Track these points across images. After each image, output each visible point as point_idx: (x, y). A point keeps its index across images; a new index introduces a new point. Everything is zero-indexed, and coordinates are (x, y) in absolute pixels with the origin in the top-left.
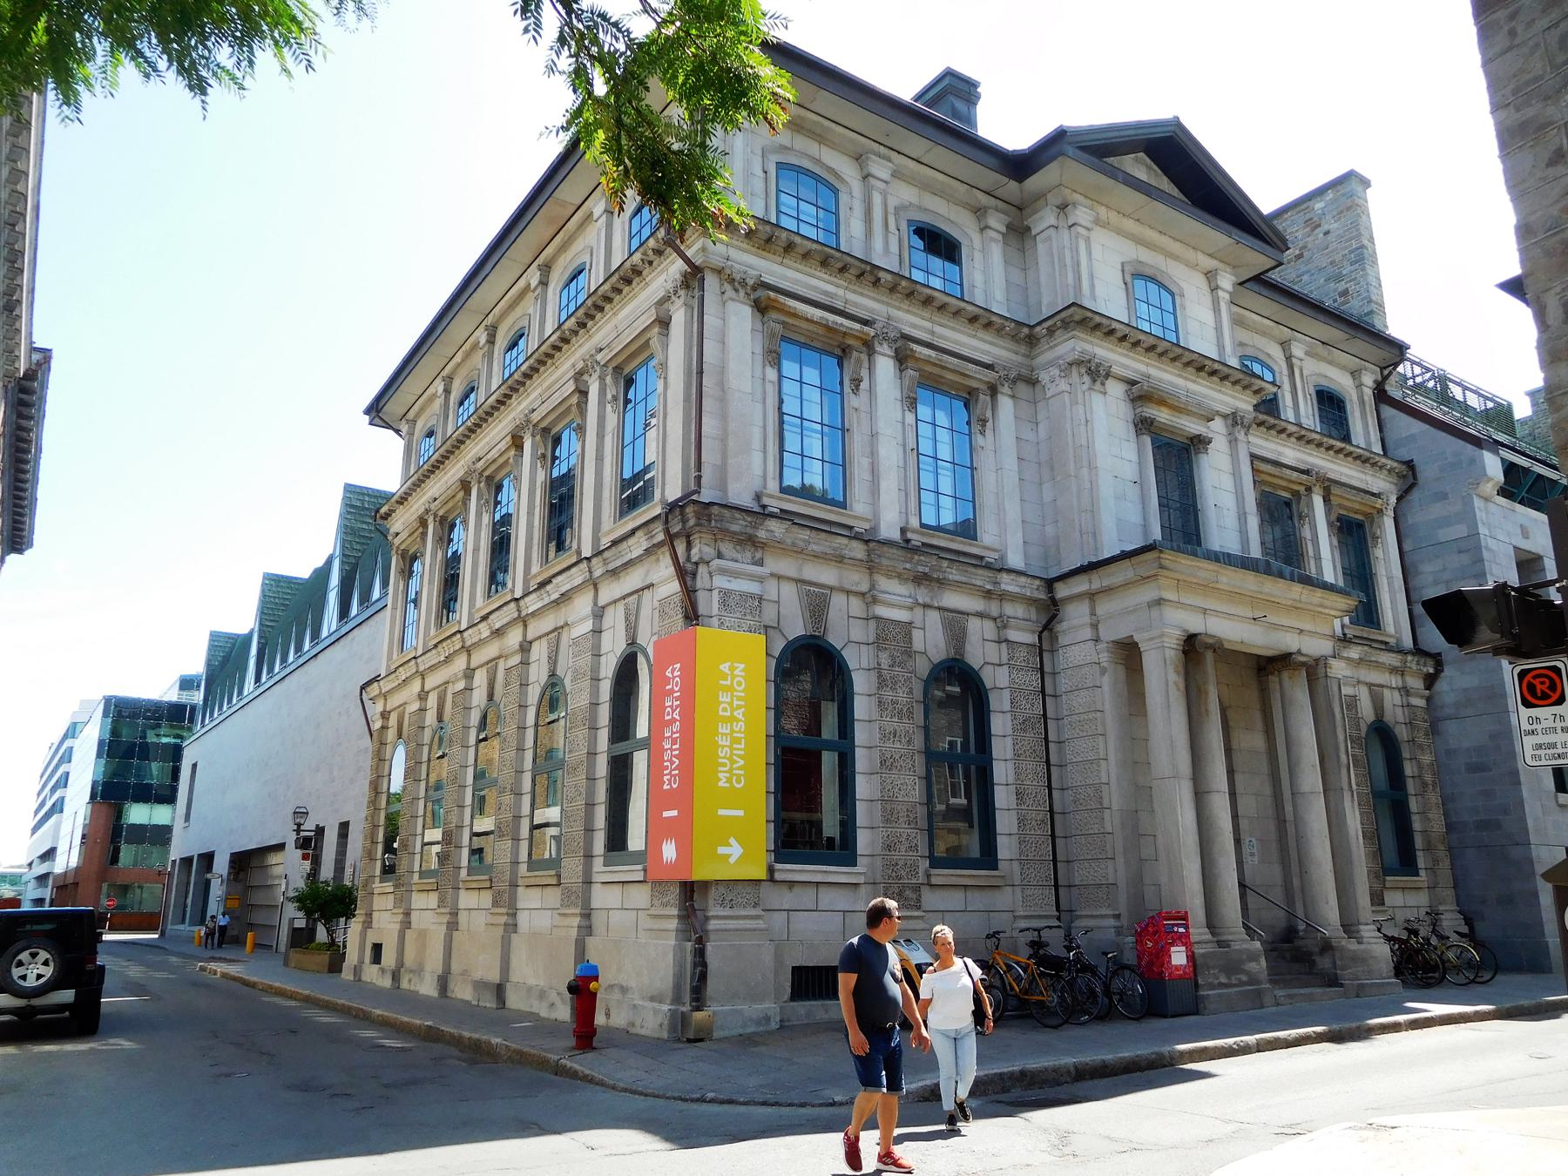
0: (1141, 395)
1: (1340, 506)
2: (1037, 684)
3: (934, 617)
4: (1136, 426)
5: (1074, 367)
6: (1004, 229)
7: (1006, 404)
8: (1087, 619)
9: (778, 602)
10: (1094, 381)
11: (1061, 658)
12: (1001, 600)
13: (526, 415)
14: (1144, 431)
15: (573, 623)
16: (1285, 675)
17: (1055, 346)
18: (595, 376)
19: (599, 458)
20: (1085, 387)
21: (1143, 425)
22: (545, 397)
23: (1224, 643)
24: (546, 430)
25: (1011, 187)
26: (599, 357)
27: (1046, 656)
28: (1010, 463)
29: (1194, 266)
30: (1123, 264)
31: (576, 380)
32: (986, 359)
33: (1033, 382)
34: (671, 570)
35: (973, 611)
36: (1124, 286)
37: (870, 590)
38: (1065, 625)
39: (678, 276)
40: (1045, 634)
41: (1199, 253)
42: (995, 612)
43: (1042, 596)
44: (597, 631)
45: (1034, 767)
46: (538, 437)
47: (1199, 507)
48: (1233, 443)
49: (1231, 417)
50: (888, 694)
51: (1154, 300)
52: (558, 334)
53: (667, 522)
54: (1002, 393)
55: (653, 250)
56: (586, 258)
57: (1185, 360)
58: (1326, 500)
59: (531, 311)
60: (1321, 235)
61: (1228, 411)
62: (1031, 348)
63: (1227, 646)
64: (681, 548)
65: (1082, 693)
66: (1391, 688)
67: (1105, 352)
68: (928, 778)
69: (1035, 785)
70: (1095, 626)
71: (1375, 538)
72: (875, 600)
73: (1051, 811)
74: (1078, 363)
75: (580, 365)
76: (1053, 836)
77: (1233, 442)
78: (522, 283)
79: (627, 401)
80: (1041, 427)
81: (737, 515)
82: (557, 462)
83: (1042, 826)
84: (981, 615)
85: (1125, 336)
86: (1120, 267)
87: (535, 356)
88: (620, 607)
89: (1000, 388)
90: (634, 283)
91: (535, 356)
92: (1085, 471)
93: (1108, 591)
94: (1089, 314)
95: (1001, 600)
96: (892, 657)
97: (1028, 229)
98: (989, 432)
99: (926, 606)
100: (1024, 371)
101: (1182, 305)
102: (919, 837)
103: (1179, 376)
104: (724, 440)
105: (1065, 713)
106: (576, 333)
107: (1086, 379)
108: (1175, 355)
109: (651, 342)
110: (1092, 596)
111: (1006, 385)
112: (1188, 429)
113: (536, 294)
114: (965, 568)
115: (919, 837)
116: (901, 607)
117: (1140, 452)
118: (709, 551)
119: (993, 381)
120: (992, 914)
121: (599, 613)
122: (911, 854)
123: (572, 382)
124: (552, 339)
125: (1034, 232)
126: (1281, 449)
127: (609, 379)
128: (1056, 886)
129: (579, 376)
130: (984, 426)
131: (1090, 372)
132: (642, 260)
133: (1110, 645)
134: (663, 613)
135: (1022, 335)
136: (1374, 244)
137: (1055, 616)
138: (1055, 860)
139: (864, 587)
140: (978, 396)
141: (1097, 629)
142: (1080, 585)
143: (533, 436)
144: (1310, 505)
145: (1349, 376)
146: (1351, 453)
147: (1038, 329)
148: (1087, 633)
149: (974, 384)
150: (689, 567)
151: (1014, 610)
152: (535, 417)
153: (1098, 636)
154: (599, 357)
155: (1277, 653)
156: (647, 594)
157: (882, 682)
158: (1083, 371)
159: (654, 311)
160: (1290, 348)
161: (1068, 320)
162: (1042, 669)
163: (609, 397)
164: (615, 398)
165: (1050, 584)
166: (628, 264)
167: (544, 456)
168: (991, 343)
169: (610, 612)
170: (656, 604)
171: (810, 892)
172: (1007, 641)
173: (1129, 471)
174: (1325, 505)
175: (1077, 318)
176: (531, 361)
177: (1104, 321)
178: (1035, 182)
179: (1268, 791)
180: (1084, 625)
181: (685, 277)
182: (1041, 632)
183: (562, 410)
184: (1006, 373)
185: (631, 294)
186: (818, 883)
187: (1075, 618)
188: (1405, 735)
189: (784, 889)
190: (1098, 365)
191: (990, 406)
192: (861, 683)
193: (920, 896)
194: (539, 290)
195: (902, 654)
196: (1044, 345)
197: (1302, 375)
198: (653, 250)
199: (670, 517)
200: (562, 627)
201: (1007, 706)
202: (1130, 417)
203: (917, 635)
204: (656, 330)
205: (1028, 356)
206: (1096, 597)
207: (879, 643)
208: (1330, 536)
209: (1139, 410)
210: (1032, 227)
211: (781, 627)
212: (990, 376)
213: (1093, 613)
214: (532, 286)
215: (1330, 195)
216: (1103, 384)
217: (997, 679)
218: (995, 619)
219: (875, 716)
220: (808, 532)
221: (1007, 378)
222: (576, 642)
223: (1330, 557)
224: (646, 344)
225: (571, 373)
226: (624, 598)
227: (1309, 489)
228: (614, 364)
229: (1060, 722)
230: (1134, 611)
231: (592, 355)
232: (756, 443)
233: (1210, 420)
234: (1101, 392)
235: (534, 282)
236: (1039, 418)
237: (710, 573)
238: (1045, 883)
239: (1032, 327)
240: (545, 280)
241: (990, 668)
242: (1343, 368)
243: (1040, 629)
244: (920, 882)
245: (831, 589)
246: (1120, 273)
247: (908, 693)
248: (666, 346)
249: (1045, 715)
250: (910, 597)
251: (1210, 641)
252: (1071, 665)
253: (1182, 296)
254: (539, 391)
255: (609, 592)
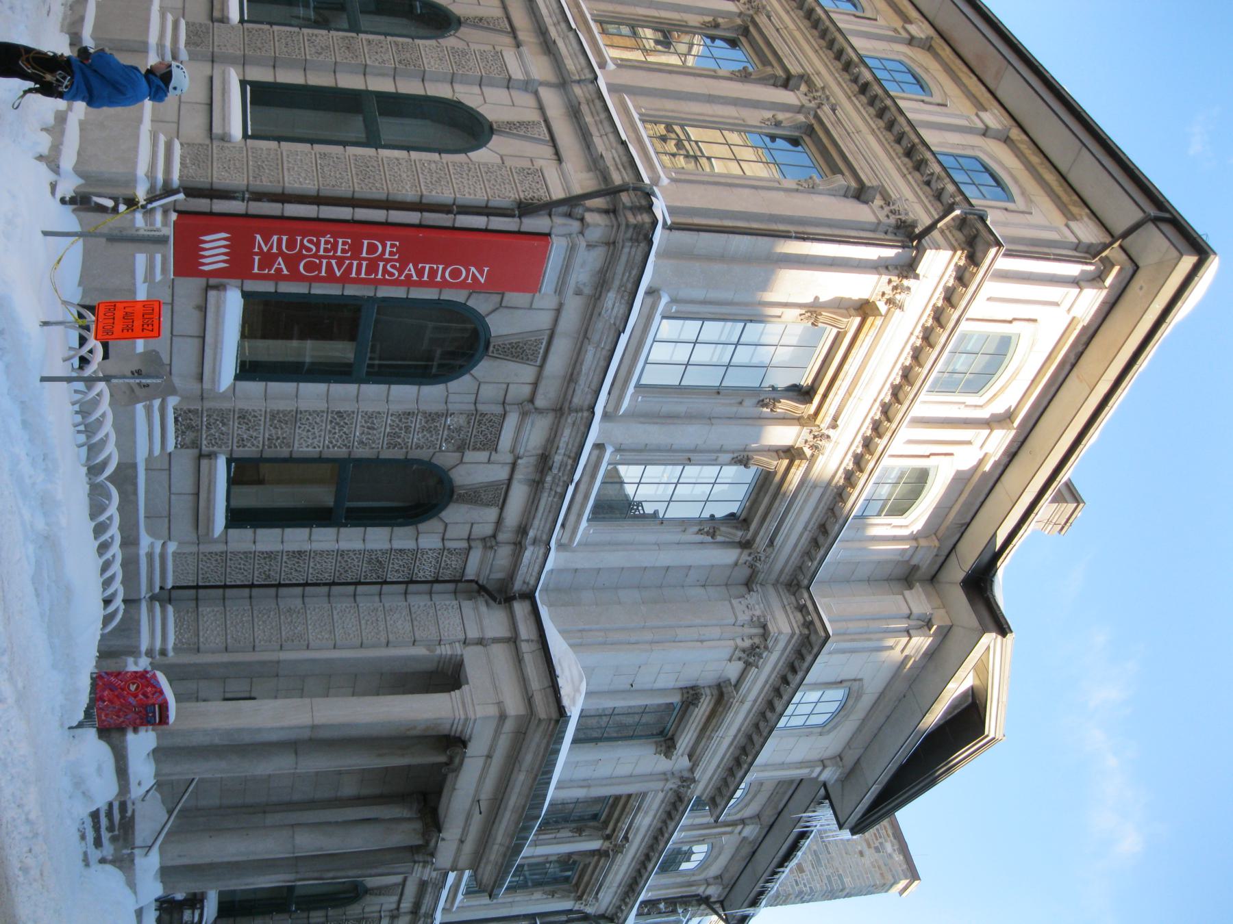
0: (722, 694)
1: (586, 866)
2: (421, 576)
3: (502, 474)
4: (693, 688)
5: (760, 631)
6: (914, 561)
7: (729, 556)
8: (490, 634)
9: (530, 308)
10: (744, 651)
11: (447, 603)
12: (515, 544)
13: (764, 7)
14: (685, 696)
15: (521, 55)
16: (418, 825)
17: (786, 612)
18: (805, 100)
19: (711, 99)
20: (739, 641)
21: (691, 695)
22: (784, 33)
23: (454, 774)
24: (746, 32)
25: (958, 571)
26: (826, 108)
27: (451, 586)
28: (665, 558)
29: (848, 745)
30: (861, 680)
31: (801, 77)
32: (778, 541)
33: (749, 584)
34: (577, 190)
35: (504, 515)
36: (839, 680)
37: (536, 409)
38: (483, 609)
39: (912, 216)
40: (475, 586)
41: (862, 751)
42: (502, 537)
43: (518, 585)
44: (509, 83)
45: (329, 570)
46: (739, 21)
47: (600, 744)
48: (663, 777)
49: (691, 776)
50: (417, 423)
51: (821, 708)
52: (855, 58)
53: (635, 189)
54: (741, 554)
55: (943, 189)
56: (1020, 203)
57: (755, 737)
58: (593, 853)
59: (881, 21)
60: (860, 848)
61: (697, 775)
62: (786, 585)
63: (450, 777)
64: (599, 202)
65: (408, 626)
66: (399, 902)
67: (772, 663)
68: (320, 460)
69: (311, 571)
70: (481, 642)
71: (553, 894)
72: (524, 414)
73: (280, 585)
74: (765, 635)
75: (819, 84)
76: (252, 586)
77: (665, 776)
78: (913, 14)
79: (773, 138)
80: (701, 591)
81: (634, 272)
82: (708, 41)
83: (264, 576)
84: (499, 522)
85: (788, 683)
86: (859, 677)
87: (831, 27)
88: (534, 116)
89: (746, 552)
90: (906, 160)
91: (831, 27)
92: (648, 636)
93: (519, 659)
94: (815, 651)
95: (515, 544)
96: (459, 430)
97: (910, 586)
98: (700, 538)
99: (514, 466)
100: (761, 577)
101: (811, 733)
102: (254, 448)
103: (739, 730)
104: (723, 258)
105: (387, 605)
106: (855, 80)
107: (747, 643)
108: (761, 728)
109: (839, 176)
110: (513, 640)
111: (750, 559)
112: (683, 736)
113: (902, 31)
114: (553, 510)
115: (254, 448)
116: (516, 440)
117: (663, 691)
118: (595, 234)
119: (755, 546)
120: (167, 520)
121: (529, 86)
122: (235, 440)
123: (800, 71)
124: (850, 50)
125: (907, 593)
126: (651, 814)
127: (801, 118)
128: (197, 587)
129: (805, 78)
130: (708, 533)
131: (754, 647)
132: (932, 174)
133: (458, 658)
134: (526, 173)
135: (801, 577)
136: (844, 897)
137: (494, 599)
138: (225, 587)
139: (540, 402)
140: (741, 529)
141: (477, 644)
142: (526, 630)
143: (740, 14)
144: (591, 838)
145: (719, 873)
146: (641, 876)
147: (806, 595)
148: (473, 634)
149: (753, 526)
150: (578, 211)
151: (503, 554)
152: (762, 20)
153: (469, 644)
154: (826, 108)
155: (441, 820)
156: (548, 151)
157: (431, 417)
158: (757, 641)
159: (875, 183)
160: (753, 824)
161: (812, 627)
162: (437, 581)
163: (781, 116)
164: (778, 124)
165: (529, 596)
166: (928, 155)
167: (717, 26)
168: (796, 545)
169: (527, 100)
170: (537, 165)
171: (192, 327)
172: (470, 548)
173: (645, 680)
174: (590, 851)
175: (813, 638)
176: (828, 23)
177: (806, 665)
178: (959, 598)
179: (297, 797)
180: (482, 629)
181: (910, 226)
182: (477, 583)
183: (765, 54)
184: (763, 559)
185: (893, 154)
186: (203, 338)
187: (493, 621)
188: (350, 912)
189: (198, 301)
190: (760, 656)
191: (727, 540)
192: (431, 395)
193: (187, 448)
194: (904, 35)
195: (463, 440)
196: (789, 599)
197: (725, 833)
198: (943, 189)
199: (639, 193)
200: (515, 37)
201: (397, 545)
202: (701, 683)
203: (482, 456)
204: (853, 184)
205: (777, 581)
206: (513, 646)
207: (476, 416)
208: (558, 854)
209: (708, 691)
210: (913, 591)
211: (501, 309)
212: (761, 542)
213: (496, 640)
214: (908, 27)
215: (898, 858)
216: (740, 659)
217: (428, 537)
218: (494, 536)
219: (394, 408)
220: (607, 348)
221: (757, 559)
222: (499, 55)
223: (536, 854)
224: (835, 170)
225: (809, 70)
226: (546, 121)
227: (608, 837)
228: (817, 127)
229: (377, 599)
230: (495, 687)
231: (828, 99)
232: (713, 295)
233: (690, 756)
234: (731, 657)
235: (913, 29)
236: (709, 589)
237: (570, 235)
238: (200, 576)
239: (808, 588)
240: (914, 42)
241: (441, 528)
242: (726, 868)
243: (480, 582)
244: (204, 447)
245: (541, 367)
246: (853, 677)
247: (417, 445)
248: (833, 193)
249: (385, 582)
250: (525, 450)
251: (457, 761)
252: (439, 613)
253: (821, 734)
254: (791, 26)
255: (553, 102)
